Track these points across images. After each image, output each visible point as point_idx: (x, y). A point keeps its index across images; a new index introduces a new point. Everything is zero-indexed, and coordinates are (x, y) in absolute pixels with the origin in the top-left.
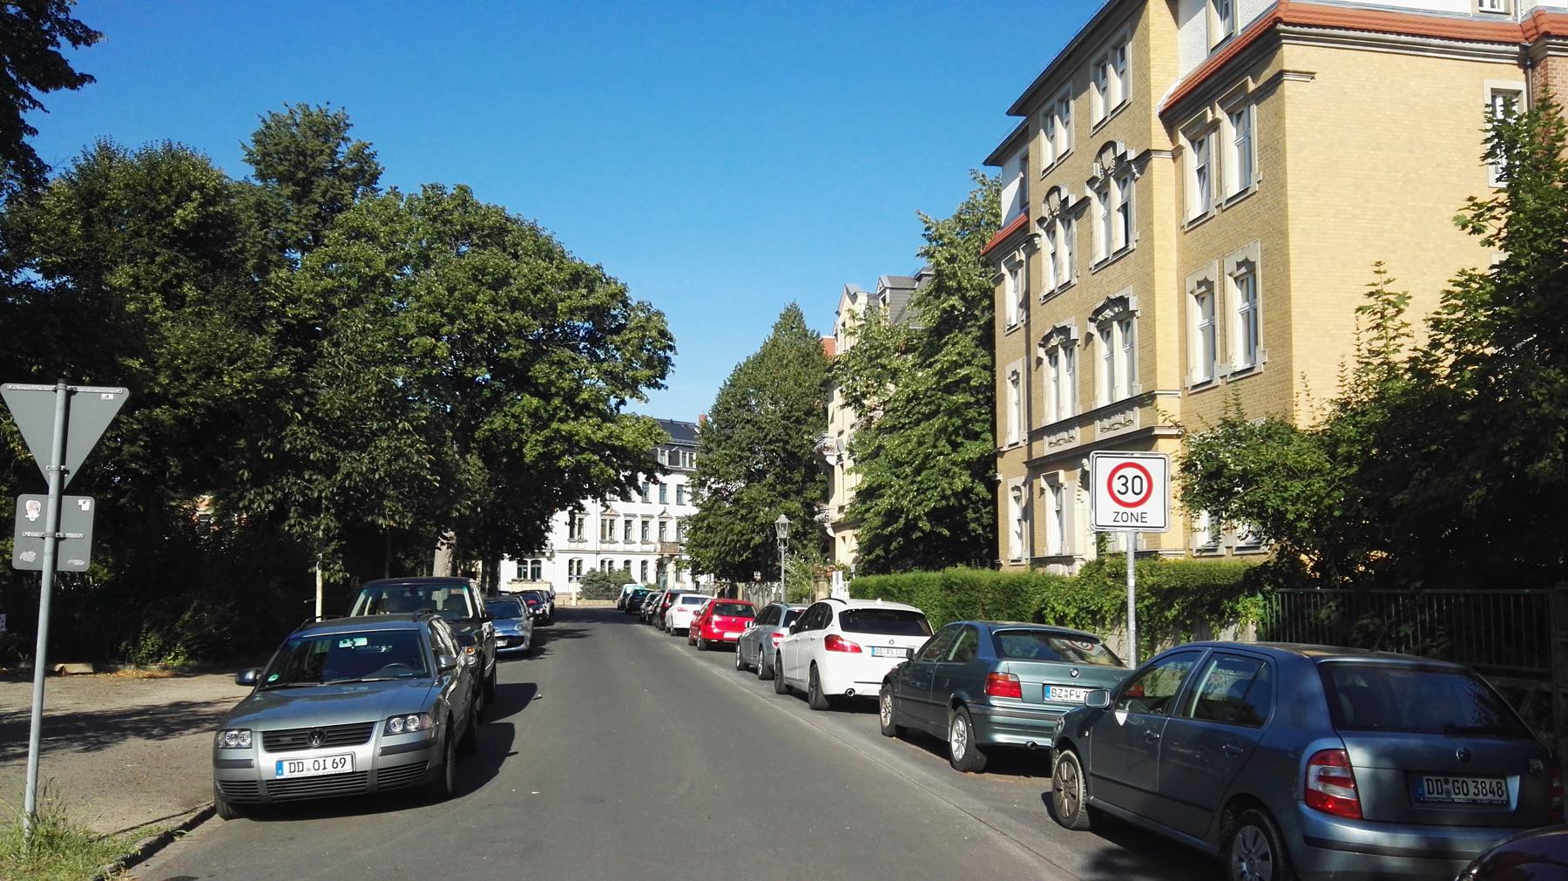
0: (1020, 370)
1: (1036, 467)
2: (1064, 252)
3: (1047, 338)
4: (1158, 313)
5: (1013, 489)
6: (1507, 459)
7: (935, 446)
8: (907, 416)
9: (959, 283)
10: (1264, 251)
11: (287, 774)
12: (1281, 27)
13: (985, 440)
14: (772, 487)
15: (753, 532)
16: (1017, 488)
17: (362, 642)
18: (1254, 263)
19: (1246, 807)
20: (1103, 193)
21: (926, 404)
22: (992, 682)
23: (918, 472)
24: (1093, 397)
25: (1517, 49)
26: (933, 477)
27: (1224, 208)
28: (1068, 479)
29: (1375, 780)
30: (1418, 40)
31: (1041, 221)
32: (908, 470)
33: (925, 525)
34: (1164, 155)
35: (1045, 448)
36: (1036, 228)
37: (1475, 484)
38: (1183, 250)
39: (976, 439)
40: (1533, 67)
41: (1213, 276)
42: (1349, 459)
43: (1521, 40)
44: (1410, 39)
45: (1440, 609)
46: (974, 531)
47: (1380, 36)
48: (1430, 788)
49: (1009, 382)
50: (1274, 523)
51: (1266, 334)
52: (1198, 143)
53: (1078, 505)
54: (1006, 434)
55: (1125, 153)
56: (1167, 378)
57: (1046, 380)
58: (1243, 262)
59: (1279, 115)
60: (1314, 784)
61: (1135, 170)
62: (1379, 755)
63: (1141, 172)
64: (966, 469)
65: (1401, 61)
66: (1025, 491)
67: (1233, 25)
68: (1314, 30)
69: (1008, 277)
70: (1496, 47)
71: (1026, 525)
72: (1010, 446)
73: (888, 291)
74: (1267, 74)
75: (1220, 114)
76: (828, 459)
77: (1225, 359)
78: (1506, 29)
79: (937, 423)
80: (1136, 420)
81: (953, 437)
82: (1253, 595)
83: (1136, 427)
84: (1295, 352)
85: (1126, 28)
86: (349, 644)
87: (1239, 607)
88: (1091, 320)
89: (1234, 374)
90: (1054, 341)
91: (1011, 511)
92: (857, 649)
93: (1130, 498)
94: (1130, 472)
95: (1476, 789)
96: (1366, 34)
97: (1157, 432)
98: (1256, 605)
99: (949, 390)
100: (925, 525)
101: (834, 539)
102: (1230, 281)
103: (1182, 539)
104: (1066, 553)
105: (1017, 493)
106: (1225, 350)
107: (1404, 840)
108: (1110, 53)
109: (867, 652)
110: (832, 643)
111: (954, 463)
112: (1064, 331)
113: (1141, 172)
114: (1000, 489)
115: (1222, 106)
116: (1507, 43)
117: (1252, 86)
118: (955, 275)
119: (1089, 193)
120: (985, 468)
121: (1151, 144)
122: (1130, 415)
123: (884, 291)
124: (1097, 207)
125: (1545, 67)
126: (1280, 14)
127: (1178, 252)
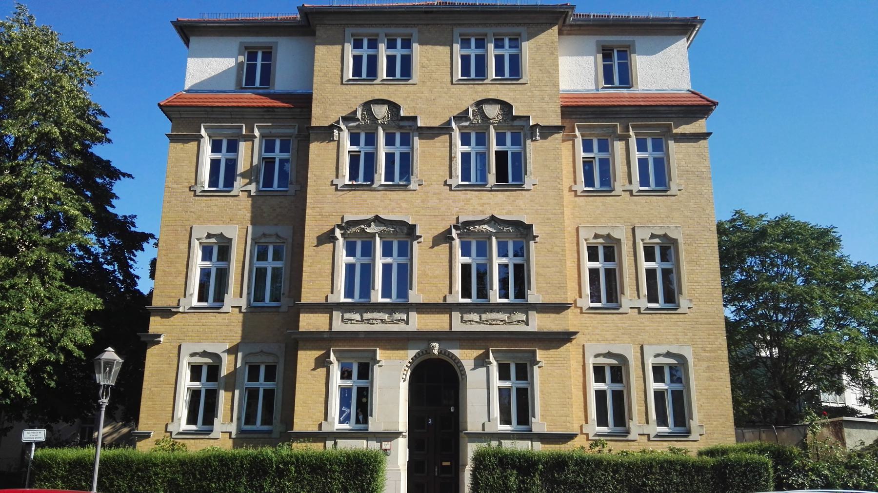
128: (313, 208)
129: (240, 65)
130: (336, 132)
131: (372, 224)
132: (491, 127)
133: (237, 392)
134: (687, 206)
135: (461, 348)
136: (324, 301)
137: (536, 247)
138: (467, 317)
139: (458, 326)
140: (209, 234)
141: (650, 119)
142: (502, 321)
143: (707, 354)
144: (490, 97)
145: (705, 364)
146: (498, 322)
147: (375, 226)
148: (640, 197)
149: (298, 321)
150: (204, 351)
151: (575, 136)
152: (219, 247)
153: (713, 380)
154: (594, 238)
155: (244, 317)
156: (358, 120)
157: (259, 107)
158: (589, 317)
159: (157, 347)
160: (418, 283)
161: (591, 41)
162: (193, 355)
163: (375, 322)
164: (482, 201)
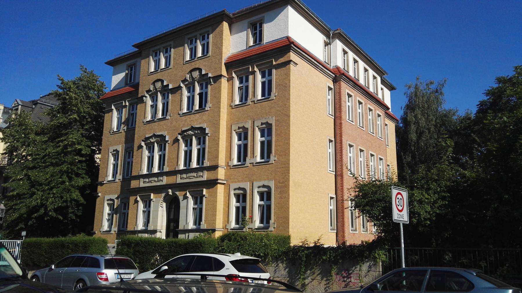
2: (160, 106)
3: (147, 139)
7: (60, 178)
9: (78, 109)
10: (277, 121)
18: (272, 124)
21: (54, 159)
23: (52, 188)
27: (111, 134)
31: (148, 92)
35: (134, 184)
36: (142, 91)
38: (229, 114)
39: (78, 177)
40: (336, 82)
41: (248, 125)
53: (160, 209)
56: (222, 161)
58: (115, 150)
59: (288, 75)
61: (212, 81)
64: (77, 189)
72: (108, 181)
73: (20, 106)
74: (281, 60)
75: (256, 69)
77: (253, 155)
79: (64, 167)
80: (205, 176)
81: (70, 175)
97: (219, 181)
102: (257, 129)
103: (222, 225)
111: (73, 186)
114: (98, 200)
117: (274, 63)
119: (182, 85)
123: (18, 106)
124: (185, 93)
127: (228, 115)
128: (137, 134)
129: (127, 74)
130: (144, 98)
131: (153, 138)
132: (196, 82)
133: (118, 215)
134: (277, 104)
135: (179, 191)
136: (174, 170)
137: (208, 138)
138: (145, 180)
139: (179, 181)
140: (239, 127)
141: (263, 60)
142: (194, 177)
143: (280, 185)
144: (196, 67)
145: (279, 190)
146: (193, 177)
147: (154, 138)
148: (258, 104)
149: (130, 184)
150: (239, 187)
151: (233, 77)
152: (244, 133)
153: (282, 198)
154: (261, 125)
155: (121, 183)
156: (151, 91)
157: (126, 93)
158: (233, 170)
159: (99, 198)
160: (167, 162)
161: (245, 23)
162: (259, 187)
163: (191, 177)
164: (191, 119)
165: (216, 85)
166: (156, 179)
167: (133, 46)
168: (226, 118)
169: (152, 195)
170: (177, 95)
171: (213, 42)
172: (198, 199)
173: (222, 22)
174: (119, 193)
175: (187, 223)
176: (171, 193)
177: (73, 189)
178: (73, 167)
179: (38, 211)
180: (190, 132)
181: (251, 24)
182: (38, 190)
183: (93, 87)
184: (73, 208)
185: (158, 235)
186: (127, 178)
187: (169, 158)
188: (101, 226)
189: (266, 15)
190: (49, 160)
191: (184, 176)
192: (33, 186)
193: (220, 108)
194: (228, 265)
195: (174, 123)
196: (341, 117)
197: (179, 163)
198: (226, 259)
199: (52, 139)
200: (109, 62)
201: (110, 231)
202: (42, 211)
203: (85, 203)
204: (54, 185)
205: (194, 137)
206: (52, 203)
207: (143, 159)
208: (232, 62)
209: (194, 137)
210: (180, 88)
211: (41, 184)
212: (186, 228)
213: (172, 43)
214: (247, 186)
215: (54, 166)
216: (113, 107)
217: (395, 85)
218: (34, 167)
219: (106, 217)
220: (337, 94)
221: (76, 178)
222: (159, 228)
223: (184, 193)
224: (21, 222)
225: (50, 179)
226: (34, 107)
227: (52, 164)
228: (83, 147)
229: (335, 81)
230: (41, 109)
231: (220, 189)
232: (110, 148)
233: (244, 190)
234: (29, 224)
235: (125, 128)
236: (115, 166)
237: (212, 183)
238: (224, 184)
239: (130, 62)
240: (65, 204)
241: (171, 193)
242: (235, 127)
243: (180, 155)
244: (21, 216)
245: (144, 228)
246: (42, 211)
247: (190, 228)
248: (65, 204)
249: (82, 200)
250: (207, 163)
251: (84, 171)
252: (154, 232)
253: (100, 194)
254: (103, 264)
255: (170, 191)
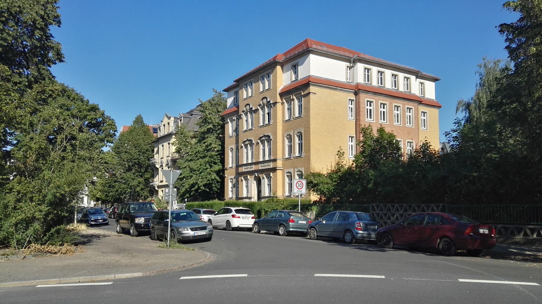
0: (233, 148)
1: (239, 174)
2: (250, 121)
3: (244, 142)
4: (278, 141)
5: (230, 179)
6: (26, 50)
7: (205, 166)
8: (196, 157)
10: (304, 131)
11: (196, 235)
12: (310, 83)
13: (219, 165)
14: (134, 174)
15: (127, 188)
16: (232, 179)
17: (185, 214)
19: (347, 230)
20: (263, 108)
21: (202, 154)
22: (290, 220)
23: (201, 173)
24: (259, 158)
25: (354, 91)
26: (205, 175)
28: (250, 178)
29: (363, 226)
30: (336, 88)
31: (243, 111)
32: (198, 173)
33: (203, 188)
34: (279, 103)
35: (243, 169)
36: (241, 112)
37: (359, 188)
38: (283, 126)
40: (357, 95)
41: (292, 134)
42: (335, 181)
43: (355, 89)
44: (334, 87)
45: (351, 208)
46: (214, 190)
47: (329, 86)
48: (368, 227)
49: (229, 150)
50: (322, 193)
51: (304, 149)
52: (287, 102)
53: (253, 184)
54: (228, 164)
55: (270, 101)
56: (279, 156)
57: (244, 152)
59: (309, 102)
60: (357, 227)
62: (363, 223)
63: (274, 106)
64: (215, 173)
65: (332, 92)
66: (234, 180)
67: (297, 77)
68: (316, 84)
69: (230, 123)
70: (350, 90)
71: (234, 189)
74: (306, 92)
75: (294, 97)
76: (156, 166)
77: (294, 153)
78: (351, 86)
79: (207, 159)
80: (271, 165)
82: (315, 206)
83: (271, 167)
84: (311, 154)
85: (270, 71)
86: (183, 214)
87: (312, 208)
88: (259, 139)
89: (296, 157)
90: (247, 143)
91: (229, 185)
92: (239, 217)
93: (299, 188)
94: (300, 183)
95: (373, 227)
96: (326, 86)
97: (277, 168)
98: (315, 208)
99: (208, 151)
100: (203, 188)
101: (158, 191)
102: (296, 136)
104: (249, 196)
105: (232, 180)
106: (294, 151)
107: (366, 232)
108: (266, 75)
109: (241, 218)
110: (233, 216)
111: (212, 171)
112: (251, 141)
113: (274, 106)
114: (226, 179)
115: (295, 96)
116: (352, 90)
117: (303, 94)
118: (211, 118)
119: (259, 108)
120: (221, 173)
121: (277, 100)
122: (269, 164)
123: (181, 118)
124: (261, 112)
125: (359, 95)
126: (310, 80)
129: (234, 98)
130: (242, 116)
139: (260, 168)
165: (274, 108)
166: (250, 167)
167: (234, 81)
168: (281, 128)
169: (248, 176)
170: (257, 114)
171: (272, 80)
172: (269, 178)
173: (276, 66)
174: (235, 175)
175: (265, 193)
176: (257, 175)
177: (212, 173)
178: (211, 159)
179: (194, 186)
180: (264, 138)
181: (293, 66)
182: (194, 174)
183: (220, 104)
184: (215, 184)
185: (253, 200)
186: (238, 166)
187: (255, 154)
188: (228, 195)
189: (300, 60)
190: (199, 155)
191: (262, 165)
192: (191, 172)
193: (277, 123)
194: (234, 211)
195: (256, 132)
196: (359, 120)
197: (260, 157)
198: (233, 209)
199: (199, 141)
200: (224, 90)
201: (290, 196)
202: (196, 187)
203: (220, 181)
204: (202, 171)
205: (266, 141)
206: (201, 183)
207: (244, 155)
208: (282, 93)
209: (266, 141)
210: (257, 110)
211: (195, 171)
212: (264, 196)
213: (253, 79)
214: (292, 170)
215: (202, 158)
216: (229, 121)
217: (437, 77)
218: (191, 160)
219: (230, 189)
220: (358, 103)
221: (214, 165)
222: (253, 196)
223: (262, 175)
224: (187, 193)
225: (199, 167)
226: (191, 117)
227: (201, 158)
228: (217, 146)
229: (356, 94)
230: (195, 118)
231: (279, 173)
232: (229, 147)
233: (290, 173)
234: (191, 194)
235: (235, 134)
236: (232, 157)
237: (274, 170)
238: (282, 170)
239: (235, 90)
240: (208, 182)
241: (257, 175)
242: (286, 135)
243: (260, 152)
244: (186, 190)
245: (269, 195)
246: (196, 187)
247: (266, 196)
248: (208, 182)
249: (218, 178)
250: (272, 158)
251: (219, 161)
252: (250, 198)
253: (226, 176)
254: (202, 212)
255: (256, 174)
